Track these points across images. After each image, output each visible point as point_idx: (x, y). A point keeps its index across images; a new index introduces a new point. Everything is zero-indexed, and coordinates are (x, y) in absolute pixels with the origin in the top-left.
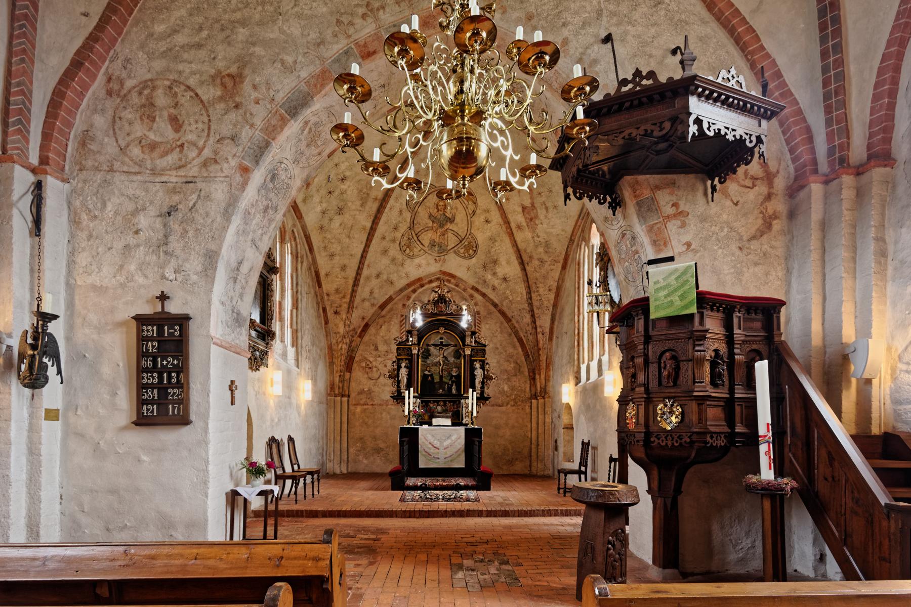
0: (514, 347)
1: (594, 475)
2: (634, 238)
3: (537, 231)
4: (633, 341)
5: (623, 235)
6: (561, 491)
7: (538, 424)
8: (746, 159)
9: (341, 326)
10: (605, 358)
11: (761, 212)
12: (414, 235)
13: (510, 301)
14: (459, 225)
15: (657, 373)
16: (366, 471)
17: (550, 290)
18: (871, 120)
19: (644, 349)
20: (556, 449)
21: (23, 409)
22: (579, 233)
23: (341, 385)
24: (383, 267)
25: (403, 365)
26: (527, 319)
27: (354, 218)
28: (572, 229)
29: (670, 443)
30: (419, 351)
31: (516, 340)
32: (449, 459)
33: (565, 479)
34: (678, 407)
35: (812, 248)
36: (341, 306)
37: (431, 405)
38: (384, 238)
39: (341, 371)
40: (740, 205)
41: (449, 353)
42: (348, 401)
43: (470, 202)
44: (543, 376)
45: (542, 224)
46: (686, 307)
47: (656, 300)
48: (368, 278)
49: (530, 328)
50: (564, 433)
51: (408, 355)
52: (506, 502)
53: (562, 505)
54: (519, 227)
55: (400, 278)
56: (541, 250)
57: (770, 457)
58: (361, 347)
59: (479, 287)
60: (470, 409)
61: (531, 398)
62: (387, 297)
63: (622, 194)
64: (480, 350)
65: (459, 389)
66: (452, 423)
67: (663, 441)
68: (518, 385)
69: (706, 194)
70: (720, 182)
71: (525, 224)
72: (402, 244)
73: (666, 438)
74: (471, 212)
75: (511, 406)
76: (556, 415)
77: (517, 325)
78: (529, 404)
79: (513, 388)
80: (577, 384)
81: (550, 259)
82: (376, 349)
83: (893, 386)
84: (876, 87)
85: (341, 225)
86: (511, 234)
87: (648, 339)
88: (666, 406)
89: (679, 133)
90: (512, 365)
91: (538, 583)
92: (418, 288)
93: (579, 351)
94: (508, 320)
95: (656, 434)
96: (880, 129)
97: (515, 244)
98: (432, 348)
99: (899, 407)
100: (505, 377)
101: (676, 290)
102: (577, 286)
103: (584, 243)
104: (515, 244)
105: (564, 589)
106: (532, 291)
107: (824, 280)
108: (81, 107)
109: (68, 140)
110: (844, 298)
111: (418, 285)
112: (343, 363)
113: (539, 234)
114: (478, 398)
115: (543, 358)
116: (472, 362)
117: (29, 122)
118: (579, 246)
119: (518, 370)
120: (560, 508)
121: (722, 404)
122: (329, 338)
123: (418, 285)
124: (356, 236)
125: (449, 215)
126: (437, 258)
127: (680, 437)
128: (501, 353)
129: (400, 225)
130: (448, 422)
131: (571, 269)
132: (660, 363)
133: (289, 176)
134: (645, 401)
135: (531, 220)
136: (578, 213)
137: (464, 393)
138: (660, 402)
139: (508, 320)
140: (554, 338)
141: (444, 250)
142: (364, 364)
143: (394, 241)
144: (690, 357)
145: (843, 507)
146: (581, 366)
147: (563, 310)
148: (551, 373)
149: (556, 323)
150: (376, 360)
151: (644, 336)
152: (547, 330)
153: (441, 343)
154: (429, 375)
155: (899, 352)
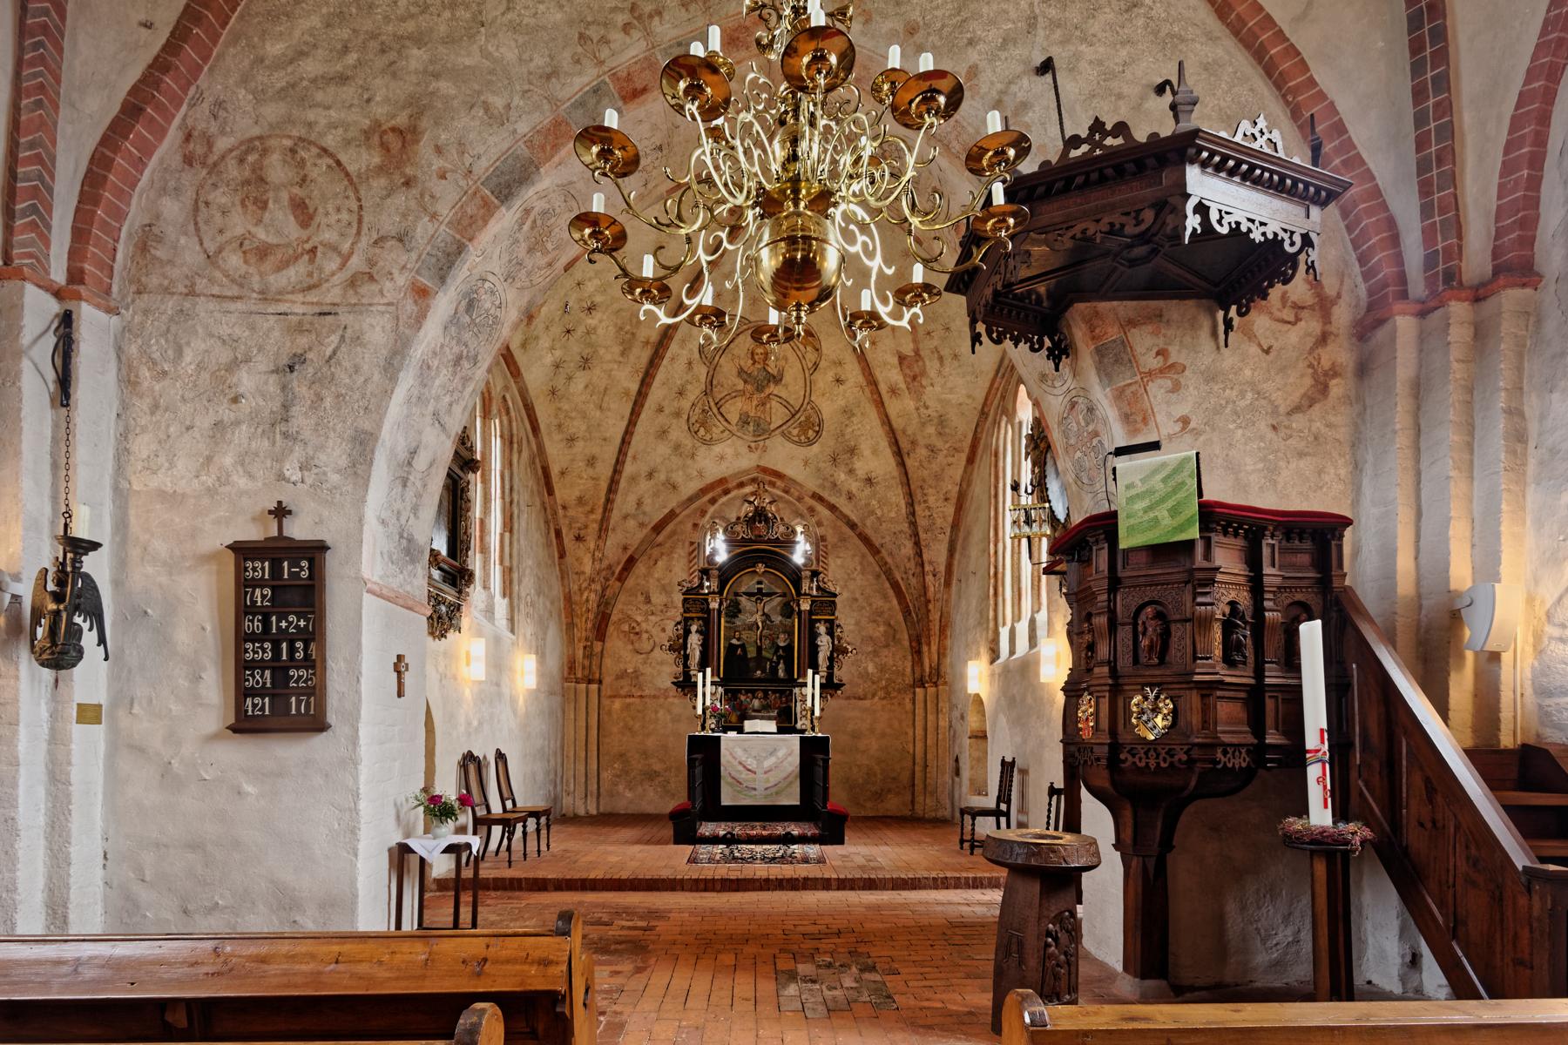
0: (885, 597)
2: (1091, 410)
3: (925, 397)
4: (1090, 587)
5: (1073, 405)
6: (966, 845)
7: (926, 730)
8: (1285, 273)
9: (587, 561)
10: (1042, 617)
11: (1311, 366)
12: (712, 404)
13: (878, 518)
14: (790, 388)
15: (1131, 643)
16: (629, 812)
17: (946, 499)
19: (1109, 601)
20: (957, 772)
21: (39, 704)
22: (996, 402)
23: (587, 663)
24: (659, 460)
25: (694, 628)
26: (908, 549)
27: (610, 376)
28: (984, 395)
29: (1152, 763)
30: (721, 604)
31: (887, 585)
32: (774, 790)
33: (973, 824)
34: (1168, 701)
35: (1398, 426)
36: (586, 527)
37: (743, 698)
38: (660, 410)
39: (587, 639)
40: (1273, 354)
41: (774, 609)
42: (599, 690)
43: (809, 348)
44: (934, 648)
45: (932, 385)
46: (1181, 528)
47: (1128, 517)
48: (633, 479)
49: (911, 565)
50: (970, 746)
51: (702, 611)
52: (872, 864)
53: (968, 869)
54: (894, 391)
55: (689, 478)
56: (931, 430)
57: (1325, 787)
58: (622, 598)
59: (825, 495)
60: (809, 703)
61: (914, 686)
62: (666, 511)
63: (1071, 334)
64: (826, 602)
65: (789, 670)
66: (778, 728)
67: (1140, 759)
68: (891, 663)
69: (1214, 334)
70: (1240, 314)
71: (903, 386)
72: (693, 420)
73: (1146, 753)
74: (810, 365)
75: (880, 699)
76: (956, 714)
77: (889, 560)
78: (911, 696)
79: (882, 669)
80: (992, 662)
81: (947, 446)
82: (648, 600)
83: (1536, 664)
84: (1508, 149)
85: (586, 387)
86: (880, 404)
87: (1114, 583)
88: (1146, 698)
89: (1169, 229)
90: (882, 629)
91: (926, 1004)
92: (720, 496)
93: (996, 604)
94: (875, 550)
95: (1128, 747)
96: (1515, 222)
97: (886, 421)
98: (743, 600)
99: (1548, 702)
100: (870, 649)
101: (1163, 500)
102: (993, 493)
103: (1004, 418)
104: (886, 421)
105: (970, 1013)
106: (916, 501)
107: (1419, 483)
108: (140, 184)
109: (117, 241)
110: (1452, 514)
111: (719, 490)
112: (590, 625)
113: (928, 403)
114: (822, 686)
115: (935, 616)
116: (812, 623)
117: (49, 210)
118: (996, 423)
119: (892, 637)
120: (965, 875)
121: (1243, 695)
122: (566, 581)
123: (719, 490)
124: (613, 406)
125: (772, 370)
126: (753, 445)
127: (1170, 753)
128: (863, 608)
129: (689, 387)
130: (772, 726)
131: (983, 462)
132: (1135, 625)
133: (497, 303)
134: (1110, 691)
135: (914, 378)
136: (995, 367)
137: (799, 677)
138: (1137, 692)
139: (875, 550)
140: (954, 582)
141: (765, 431)
142: (626, 627)
143: (677, 414)
144: (1188, 615)
145: (1452, 872)
146: (1001, 629)
147: (968, 533)
148: (948, 642)
149: (957, 556)
150: (647, 620)
151: (1109, 578)
152: (942, 568)
153: (760, 590)
154: (738, 646)
155: (1548, 605)
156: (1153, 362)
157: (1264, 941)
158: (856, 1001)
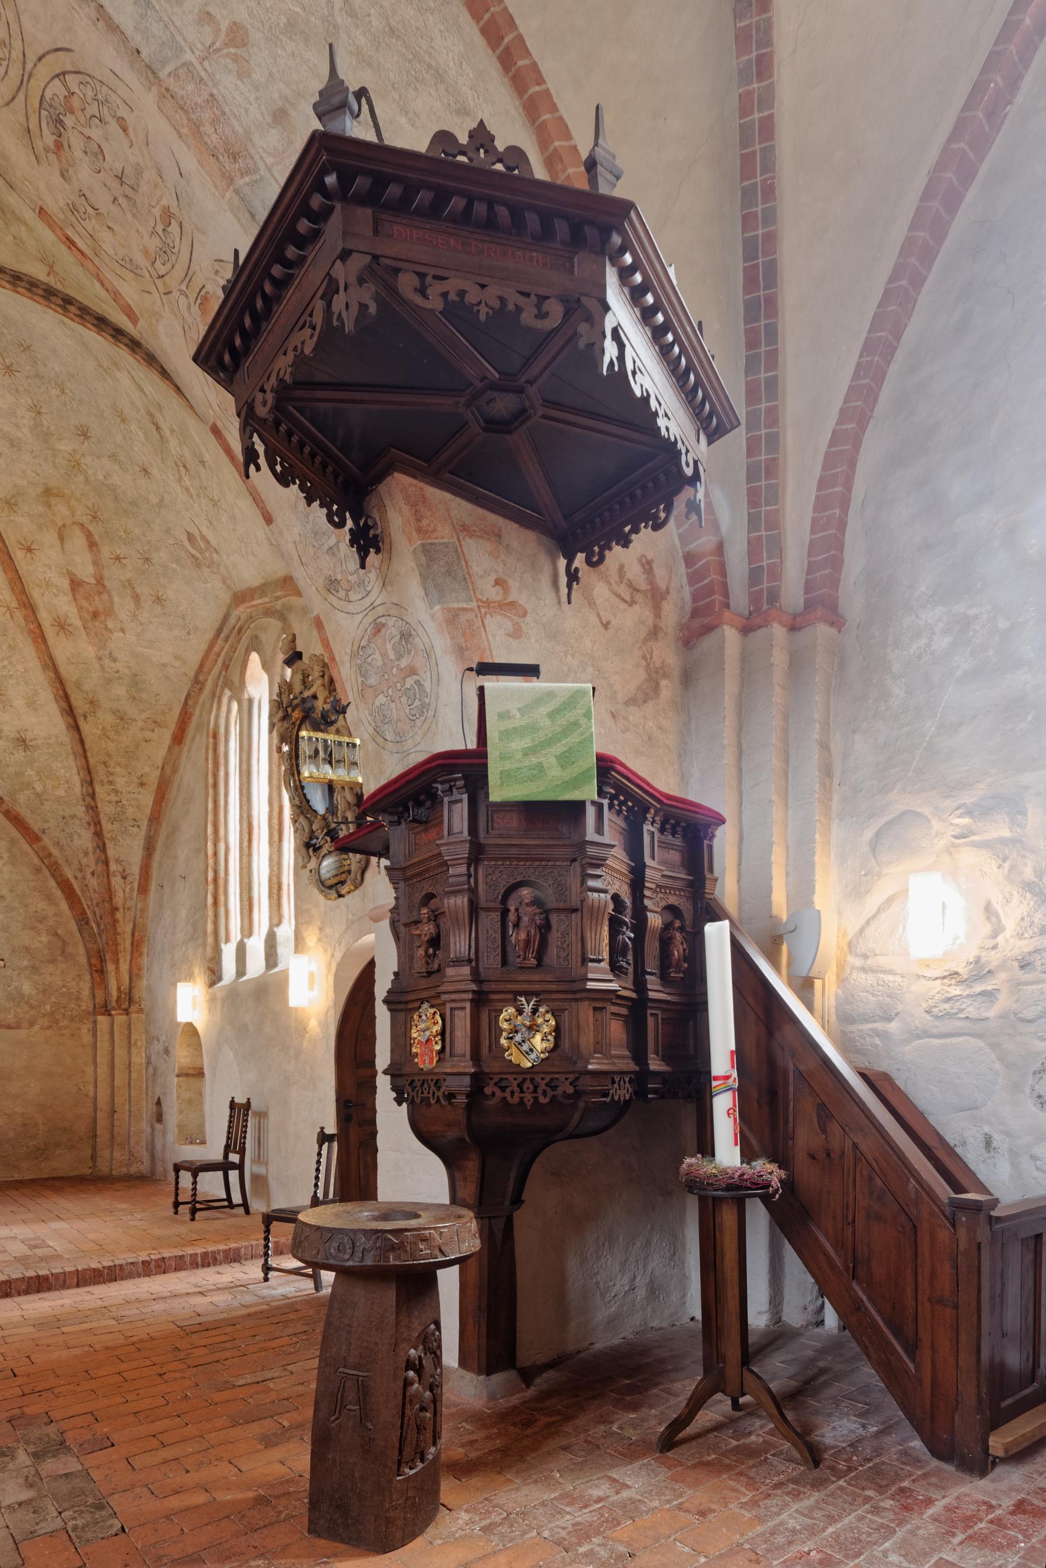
0: (49, 898)
1: (260, 1170)
2: (406, 636)
4: (440, 854)
5: (378, 628)
6: (184, 1209)
7: (112, 1067)
8: (656, 517)
10: (286, 931)
11: (644, 657)
13: (38, 795)
15: (498, 936)
17: (142, 785)
18: (811, 540)
19: (469, 876)
20: (159, 1117)
22: (215, 671)
26: (85, 839)
28: (198, 658)
29: (528, 1099)
31: (52, 883)
33: (195, 1183)
34: (549, 1016)
35: (726, 741)
40: (611, 631)
44: (124, 967)
45: (123, 630)
46: (575, 783)
47: (503, 757)
49: (90, 862)
50: (179, 1086)
52: (39, 1252)
53: (192, 1242)
54: (62, 626)
56: (119, 690)
57: (735, 1119)
61: (95, 1012)
63: (385, 520)
67: (512, 1093)
68: (60, 983)
69: (555, 583)
70: (589, 562)
73: (520, 1086)
75: (43, 1028)
76: (158, 1047)
77: (55, 852)
79: (46, 990)
80: (212, 984)
81: (144, 716)
83: (840, 992)
84: (822, 483)
86: (39, 637)
87: (477, 853)
88: (520, 1011)
89: (582, 343)
90: (44, 938)
91: (175, 1502)
93: (216, 916)
94: (32, 837)
95: (496, 1078)
96: (826, 559)
97: (50, 664)
99: (850, 1028)
100: (25, 963)
101: (549, 742)
102: (211, 781)
103: (227, 693)
104: (50, 664)
105: (261, 1501)
107: (741, 805)
110: (774, 839)
113: (116, 654)
115: (125, 928)
118: (216, 697)
119: (61, 949)
120: (190, 1251)
121: (624, 1011)
127: (552, 1085)
128: (12, 909)
131: (196, 746)
132: (505, 912)
134: (472, 1001)
135: (95, 615)
136: (217, 625)
138: (508, 1002)
139: (32, 837)
140: (153, 886)
144: (575, 902)
145: (851, 1208)
146: (223, 946)
147: (174, 830)
148: (145, 961)
149: (157, 857)
151: (471, 842)
152: (135, 870)
155: (849, 937)
156: (493, 593)
157: (603, 1295)
158: (32, 1535)
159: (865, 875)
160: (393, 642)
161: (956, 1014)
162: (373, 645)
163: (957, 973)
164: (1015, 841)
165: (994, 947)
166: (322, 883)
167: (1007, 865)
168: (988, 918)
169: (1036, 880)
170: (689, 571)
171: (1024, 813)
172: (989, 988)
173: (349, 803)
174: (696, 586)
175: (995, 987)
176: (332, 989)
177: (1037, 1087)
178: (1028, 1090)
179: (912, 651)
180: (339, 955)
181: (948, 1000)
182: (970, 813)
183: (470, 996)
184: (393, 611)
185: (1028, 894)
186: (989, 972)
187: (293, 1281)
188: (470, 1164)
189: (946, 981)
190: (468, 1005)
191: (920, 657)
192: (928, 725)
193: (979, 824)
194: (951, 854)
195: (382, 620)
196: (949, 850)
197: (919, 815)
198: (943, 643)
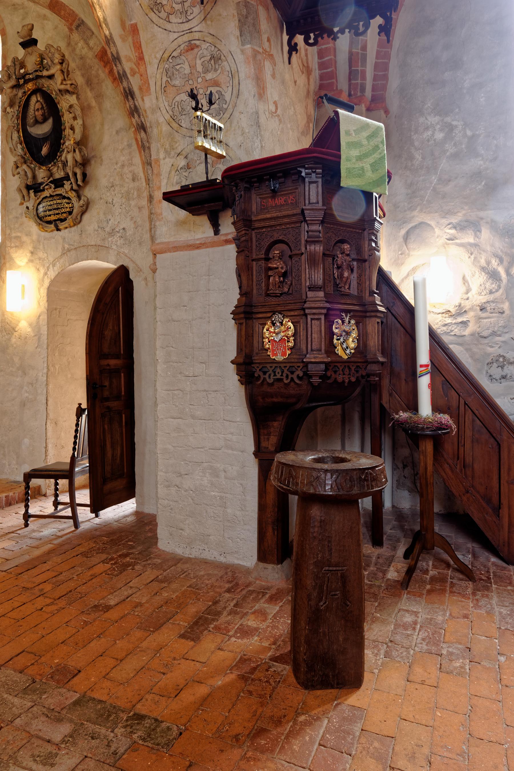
5: (191, 47)
101: (366, 155)
159: (401, 254)
160: (203, 60)
161: (449, 333)
162: (183, 57)
163: (449, 311)
164: (476, 245)
165: (468, 299)
166: (40, 218)
167: (472, 257)
168: (464, 283)
169: (487, 266)
170: (320, 61)
171: (480, 231)
172: (465, 320)
173: (76, 161)
174: (322, 71)
175: (467, 319)
176: (45, 299)
177: (489, 371)
178: (485, 373)
179: (424, 137)
180: (52, 274)
181: (445, 325)
182: (455, 228)
183: (324, 311)
184: (209, 39)
185: (483, 273)
186: (465, 311)
187: (49, 523)
188: (276, 424)
189: (444, 315)
190: (323, 317)
191: (428, 141)
192: (433, 178)
193: (460, 234)
194: (445, 248)
195: (197, 42)
196: (445, 245)
197: (429, 225)
198: (439, 136)
